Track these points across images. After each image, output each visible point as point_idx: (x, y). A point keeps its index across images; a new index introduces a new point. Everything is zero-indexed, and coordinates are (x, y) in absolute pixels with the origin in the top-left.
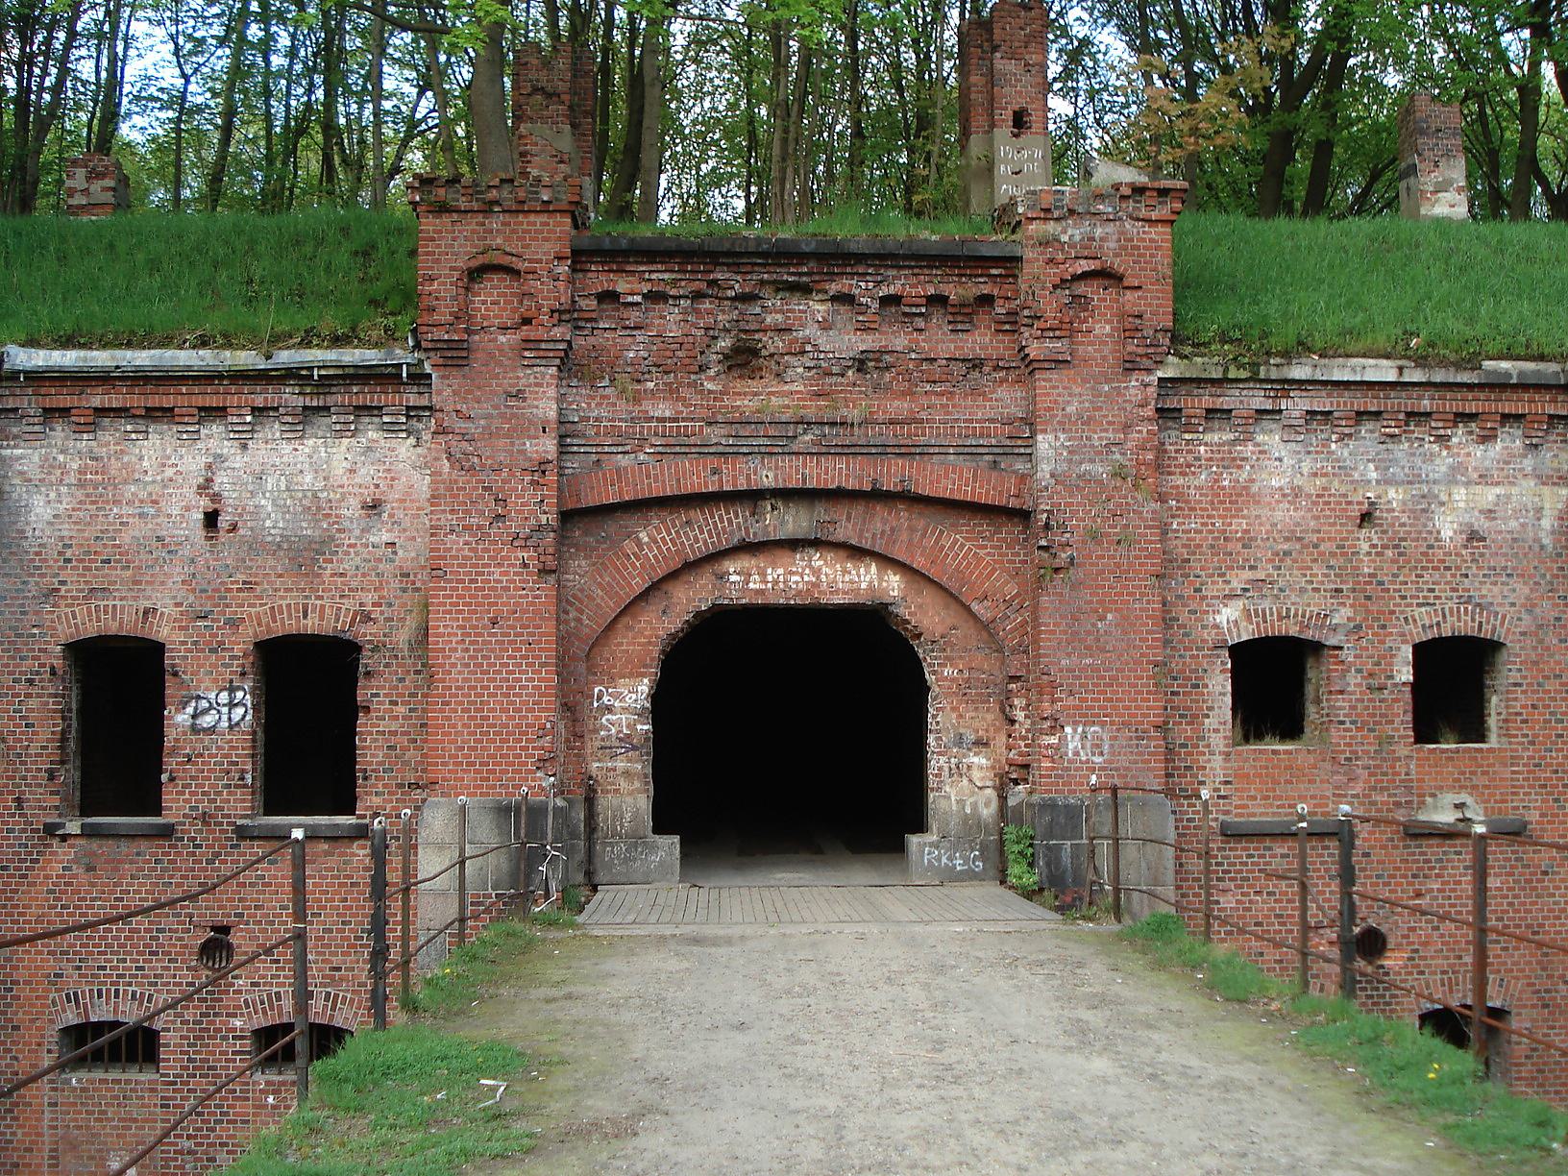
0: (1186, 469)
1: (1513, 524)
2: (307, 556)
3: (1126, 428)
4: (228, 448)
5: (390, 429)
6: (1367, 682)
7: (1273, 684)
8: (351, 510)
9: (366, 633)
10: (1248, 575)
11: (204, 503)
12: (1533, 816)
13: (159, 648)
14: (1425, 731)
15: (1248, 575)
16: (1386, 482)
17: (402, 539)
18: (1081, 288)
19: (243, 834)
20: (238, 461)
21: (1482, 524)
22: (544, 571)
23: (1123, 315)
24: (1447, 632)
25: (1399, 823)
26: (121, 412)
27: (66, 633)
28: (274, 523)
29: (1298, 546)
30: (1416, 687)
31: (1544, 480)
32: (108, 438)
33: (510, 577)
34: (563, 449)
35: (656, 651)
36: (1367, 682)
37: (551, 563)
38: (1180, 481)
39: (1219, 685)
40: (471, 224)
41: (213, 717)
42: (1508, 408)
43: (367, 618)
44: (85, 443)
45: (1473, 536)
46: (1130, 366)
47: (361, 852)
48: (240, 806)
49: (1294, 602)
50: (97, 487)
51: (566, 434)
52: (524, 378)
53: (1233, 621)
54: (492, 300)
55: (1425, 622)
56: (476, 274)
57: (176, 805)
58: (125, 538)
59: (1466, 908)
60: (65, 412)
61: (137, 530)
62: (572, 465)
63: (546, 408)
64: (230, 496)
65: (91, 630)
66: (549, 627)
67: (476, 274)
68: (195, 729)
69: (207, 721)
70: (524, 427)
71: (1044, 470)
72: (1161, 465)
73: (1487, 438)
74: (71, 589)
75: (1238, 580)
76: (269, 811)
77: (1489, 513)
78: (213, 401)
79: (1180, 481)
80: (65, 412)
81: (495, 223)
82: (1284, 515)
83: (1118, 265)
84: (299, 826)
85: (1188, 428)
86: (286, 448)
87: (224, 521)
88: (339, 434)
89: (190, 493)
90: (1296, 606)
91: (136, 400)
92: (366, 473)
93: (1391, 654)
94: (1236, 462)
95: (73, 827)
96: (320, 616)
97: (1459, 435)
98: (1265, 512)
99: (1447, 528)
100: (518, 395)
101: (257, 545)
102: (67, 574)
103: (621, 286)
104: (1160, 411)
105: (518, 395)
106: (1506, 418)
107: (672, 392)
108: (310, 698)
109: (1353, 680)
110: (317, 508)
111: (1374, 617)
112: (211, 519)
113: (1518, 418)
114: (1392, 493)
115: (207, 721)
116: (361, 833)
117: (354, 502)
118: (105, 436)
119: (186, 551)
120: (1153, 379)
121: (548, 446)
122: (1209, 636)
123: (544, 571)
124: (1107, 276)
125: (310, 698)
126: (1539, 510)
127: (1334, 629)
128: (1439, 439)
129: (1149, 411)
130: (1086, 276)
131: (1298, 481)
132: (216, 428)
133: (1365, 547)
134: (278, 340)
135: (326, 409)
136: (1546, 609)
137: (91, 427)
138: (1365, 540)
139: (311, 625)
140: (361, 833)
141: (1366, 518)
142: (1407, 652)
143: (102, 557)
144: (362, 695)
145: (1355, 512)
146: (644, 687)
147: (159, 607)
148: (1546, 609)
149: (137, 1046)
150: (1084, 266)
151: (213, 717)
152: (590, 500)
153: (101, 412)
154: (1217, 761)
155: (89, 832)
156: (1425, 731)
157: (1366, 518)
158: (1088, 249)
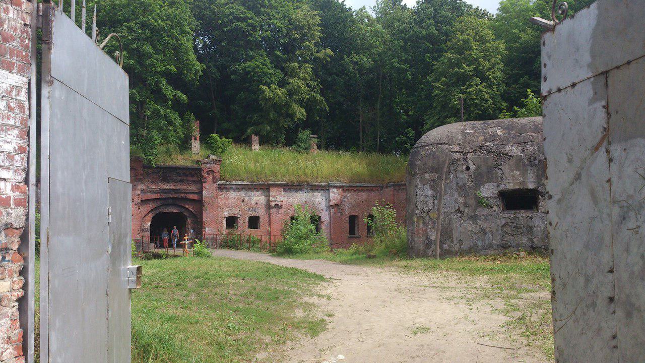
6: (243, 222)
7: (232, 221)
25: (413, 239)
29: (235, 205)
30: (249, 222)
36: (243, 222)
39: (225, 222)
46: (214, 182)
49: (234, 212)
53: (226, 214)
55: (250, 214)
82: (233, 201)
83: (213, 169)
84: (436, 237)
90: (236, 212)
99: (253, 202)
124: (212, 171)
134: (112, 215)
141: (243, 201)
142: (248, 218)
145: (242, 200)
146: (150, 224)
149: (180, 285)
156: (250, 227)
157: (243, 201)
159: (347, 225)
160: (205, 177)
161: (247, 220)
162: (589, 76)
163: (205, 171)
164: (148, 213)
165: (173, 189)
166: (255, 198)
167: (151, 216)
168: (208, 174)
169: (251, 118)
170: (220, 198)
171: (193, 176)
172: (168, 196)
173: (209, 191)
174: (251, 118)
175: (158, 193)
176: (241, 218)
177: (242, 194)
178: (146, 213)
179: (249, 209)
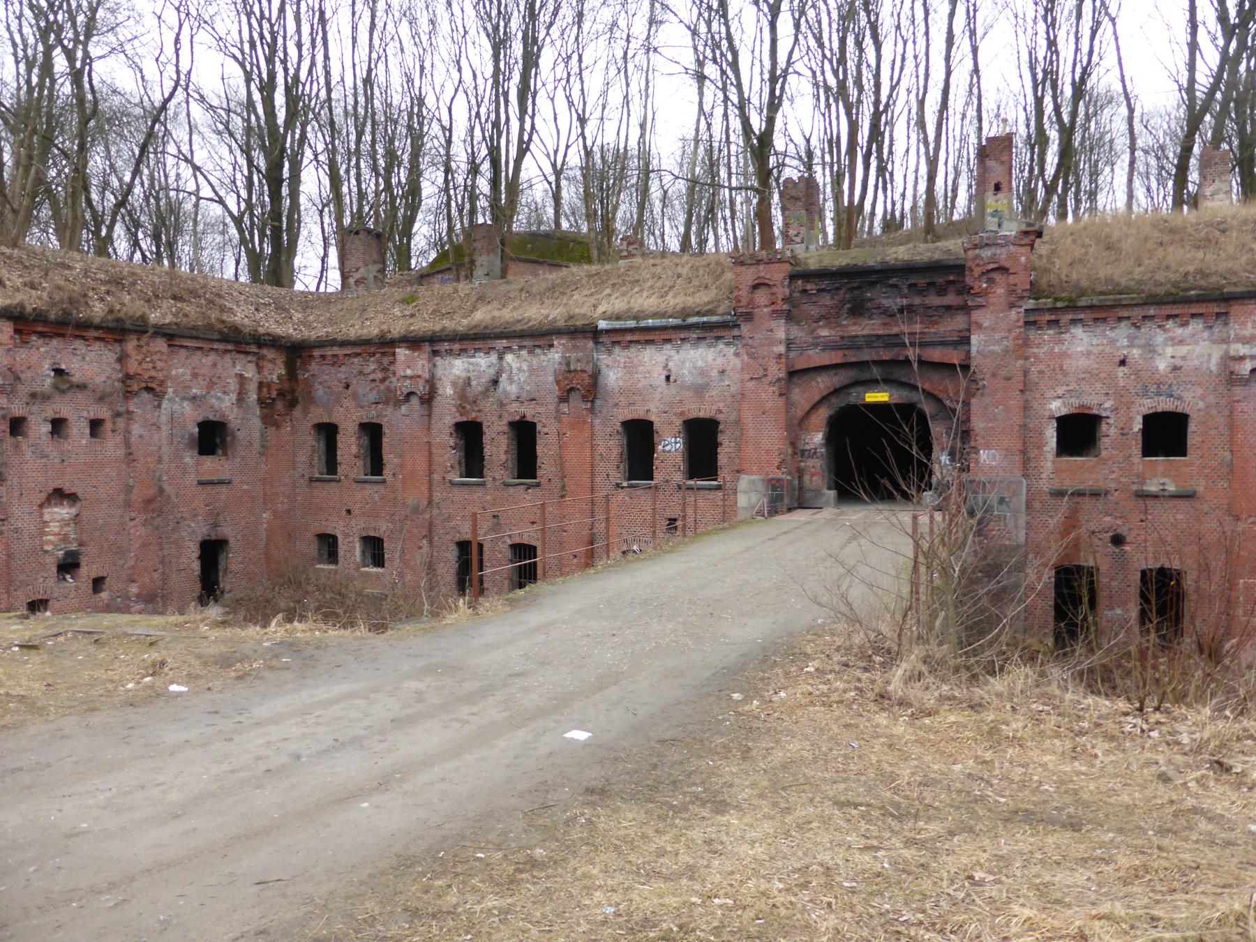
0: (1039, 346)
1: (1196, 362)
2: (699, 391)
3: (1010, 331)
4: (673, 353)
5: (727, 344)
7: (1078, 433)
8: (714, 374)
9: (720, 417)
10: (1065, 388)
11: (665, 373)
12: (1200, 489)
13: (651, 423)
14: (1148, 450)
15: (1065, 388)
16: (1131, 346)
17: (732, 383)
18: (992, 275)
19: (507, 485)
20: (676, 357)
21: (1179, 362)
22: (781, 395)
23: (1009, 285)
24: (1159, 410)
26: (638, 342)
27: (622, 419)
28: (689, 379)
31: (1213, 342)
32: (633, 351)
33: (768, 396)
34: (788, 348)
35: (825, 422)
37: (784, 391)
38: (1036, 350)
39: (1051, 435)
40: (752, 269)
41: (671, 446)
42: (1194, 311)
43: (720, 412)
44: (626, 353)
45: (1176, 368)
46: (1012, 306)
47: (720, 494)
48: (678, 478)
50: (630, 368)
51: (789, 343)
52: (773, 324)
53: (1058, 407)
54: (762, 297)
56: (755, 287)
57: (659, 476)
58: (640, 385)
59: (589, 485)
60: (618, 342)
61: (644, 383)
62: (792, 355)
63: (781, 334)
64: (674, 370)
65: (629, 417)
66: (783, 415)
67: (755, 287)
68: (664, 451)
69: (668, 448)
70: (773, 342)
71: (974, 349)
72: (1026, 343)
73: (1184, 325)
74: (622, 404)
75: (1060, 391)
76: (691, 478)
77: (1184, 358)
78: (667, 337)
79: (1036, 350)
80: (618, 342)
81: (761, 267)
82: (1083, 362)
83: (1007, 264)
85: (1040, 328)
86: (692, 352)
87: (672, 379)
88: (710, 347)
89: (660, 369)
90: (1095, 399)
91: (642, 337)
92: (720, 360)
93: (1131, 419)
94: (1061, 342)
95: (625, 484)
96: (703, 411)
97: (1170, 324)
98: (1074, 362)
99: (1162, 365)
100: (771, 330)
101: (683, 387)
102: (622, 399)
103: (809, 287)
104: (1026, 323)
105: (771, 330)
106: (1193, 316)
107: (828, 326)
108: (703, 440)
109: (1113, 431)
110: (703, 373)
111: (1125, 403)
112: (668, 378)
113: (1201, 315)
114: (1135, 351)
115: (668, 448)
116: (719, 488)
117: (715, 371)
118: (633, 350)
119: (659, 390)
120: (1022, 310)
121: (782, 349)
122: (1047, 414)
123: (781, 395)
124: (1003, 269)
125: (703, 440)
126: (1210, 356)
127: (1106, 409)
128: (1160, 326)
129: (1021, 323)
130: (993, 270)
131: (1090, 348)
132: (669, 346)
133: (1121, 374)
135: (704, 338)
136: (1212, 399)
137: (627, 347)
138: (1121, 371)
139: (702, 415)
140: (719, 488)
141: (1123, 363)
142: (1140, 419)
143: (630, 392)
144: (719, 440)
145: (1117, 360)
147: (652, 409)
148: (1212, 399)
150: (992, 266)
151: (671, 446)
152: (799, 367)
153: (631, 342)
154: (1049, 464)
155: (630, 486)
156: (1148, 450)
157: (1123, 363)
158: (993, 259)
159: (196, 566)
160: (977, 290)
161: (1138, 426)
162: (855, 606)
163: (977, 271)
164: (816, 406)
165: (878, 337)
166: (1169, 351)
167: (824, 413)
168: (991, 281)
169: (1203, 398)
170: (1036, 356)
171: (942, 292)
172: (866, 355)
173: (990, 335)
174: (1203, 398)
175: (840, 348)
176: (1111, 421)
177: (1119, 337)
178: (808, 406)
179: (1145, 387)
